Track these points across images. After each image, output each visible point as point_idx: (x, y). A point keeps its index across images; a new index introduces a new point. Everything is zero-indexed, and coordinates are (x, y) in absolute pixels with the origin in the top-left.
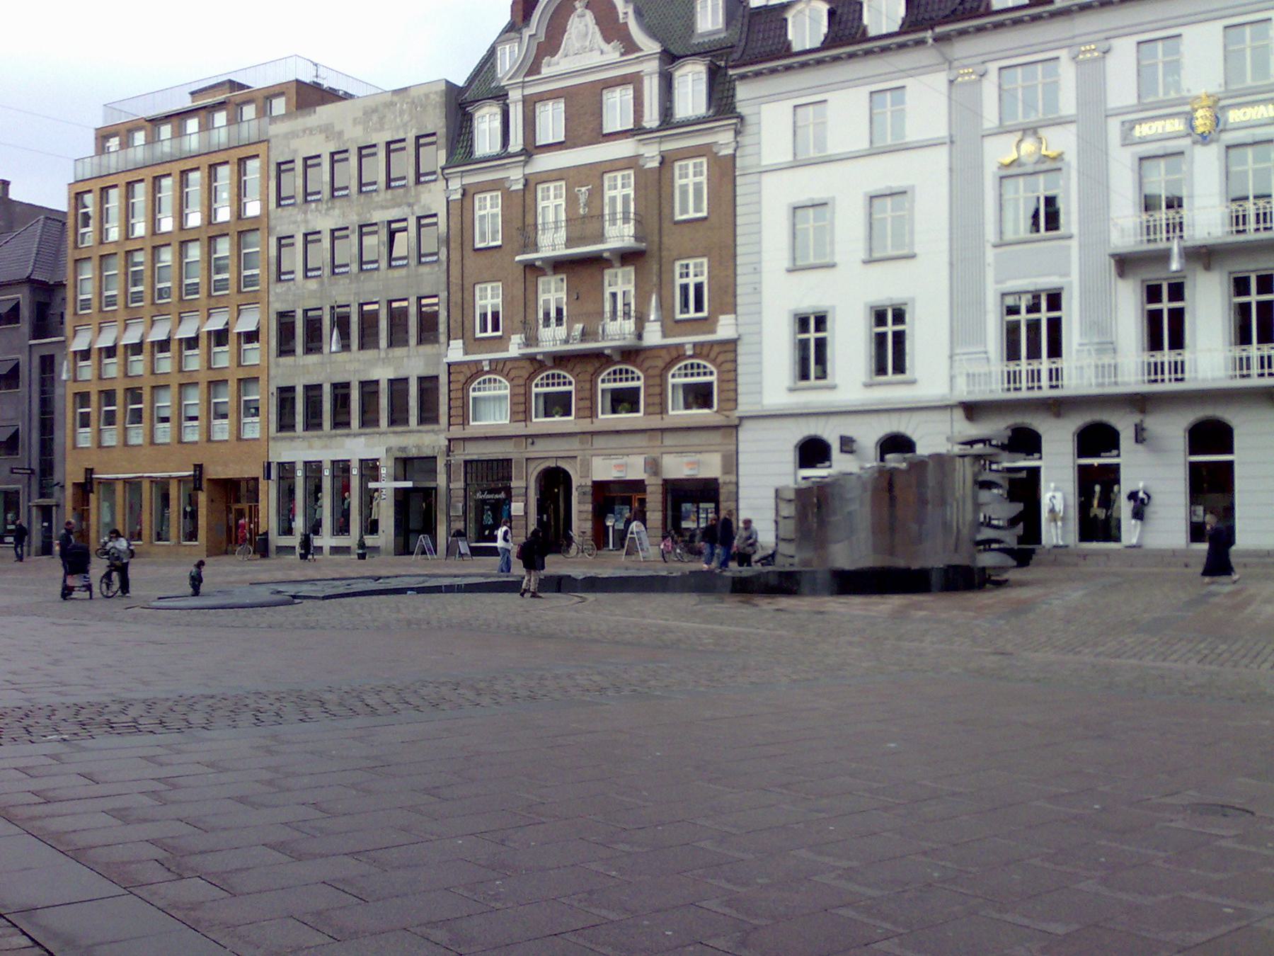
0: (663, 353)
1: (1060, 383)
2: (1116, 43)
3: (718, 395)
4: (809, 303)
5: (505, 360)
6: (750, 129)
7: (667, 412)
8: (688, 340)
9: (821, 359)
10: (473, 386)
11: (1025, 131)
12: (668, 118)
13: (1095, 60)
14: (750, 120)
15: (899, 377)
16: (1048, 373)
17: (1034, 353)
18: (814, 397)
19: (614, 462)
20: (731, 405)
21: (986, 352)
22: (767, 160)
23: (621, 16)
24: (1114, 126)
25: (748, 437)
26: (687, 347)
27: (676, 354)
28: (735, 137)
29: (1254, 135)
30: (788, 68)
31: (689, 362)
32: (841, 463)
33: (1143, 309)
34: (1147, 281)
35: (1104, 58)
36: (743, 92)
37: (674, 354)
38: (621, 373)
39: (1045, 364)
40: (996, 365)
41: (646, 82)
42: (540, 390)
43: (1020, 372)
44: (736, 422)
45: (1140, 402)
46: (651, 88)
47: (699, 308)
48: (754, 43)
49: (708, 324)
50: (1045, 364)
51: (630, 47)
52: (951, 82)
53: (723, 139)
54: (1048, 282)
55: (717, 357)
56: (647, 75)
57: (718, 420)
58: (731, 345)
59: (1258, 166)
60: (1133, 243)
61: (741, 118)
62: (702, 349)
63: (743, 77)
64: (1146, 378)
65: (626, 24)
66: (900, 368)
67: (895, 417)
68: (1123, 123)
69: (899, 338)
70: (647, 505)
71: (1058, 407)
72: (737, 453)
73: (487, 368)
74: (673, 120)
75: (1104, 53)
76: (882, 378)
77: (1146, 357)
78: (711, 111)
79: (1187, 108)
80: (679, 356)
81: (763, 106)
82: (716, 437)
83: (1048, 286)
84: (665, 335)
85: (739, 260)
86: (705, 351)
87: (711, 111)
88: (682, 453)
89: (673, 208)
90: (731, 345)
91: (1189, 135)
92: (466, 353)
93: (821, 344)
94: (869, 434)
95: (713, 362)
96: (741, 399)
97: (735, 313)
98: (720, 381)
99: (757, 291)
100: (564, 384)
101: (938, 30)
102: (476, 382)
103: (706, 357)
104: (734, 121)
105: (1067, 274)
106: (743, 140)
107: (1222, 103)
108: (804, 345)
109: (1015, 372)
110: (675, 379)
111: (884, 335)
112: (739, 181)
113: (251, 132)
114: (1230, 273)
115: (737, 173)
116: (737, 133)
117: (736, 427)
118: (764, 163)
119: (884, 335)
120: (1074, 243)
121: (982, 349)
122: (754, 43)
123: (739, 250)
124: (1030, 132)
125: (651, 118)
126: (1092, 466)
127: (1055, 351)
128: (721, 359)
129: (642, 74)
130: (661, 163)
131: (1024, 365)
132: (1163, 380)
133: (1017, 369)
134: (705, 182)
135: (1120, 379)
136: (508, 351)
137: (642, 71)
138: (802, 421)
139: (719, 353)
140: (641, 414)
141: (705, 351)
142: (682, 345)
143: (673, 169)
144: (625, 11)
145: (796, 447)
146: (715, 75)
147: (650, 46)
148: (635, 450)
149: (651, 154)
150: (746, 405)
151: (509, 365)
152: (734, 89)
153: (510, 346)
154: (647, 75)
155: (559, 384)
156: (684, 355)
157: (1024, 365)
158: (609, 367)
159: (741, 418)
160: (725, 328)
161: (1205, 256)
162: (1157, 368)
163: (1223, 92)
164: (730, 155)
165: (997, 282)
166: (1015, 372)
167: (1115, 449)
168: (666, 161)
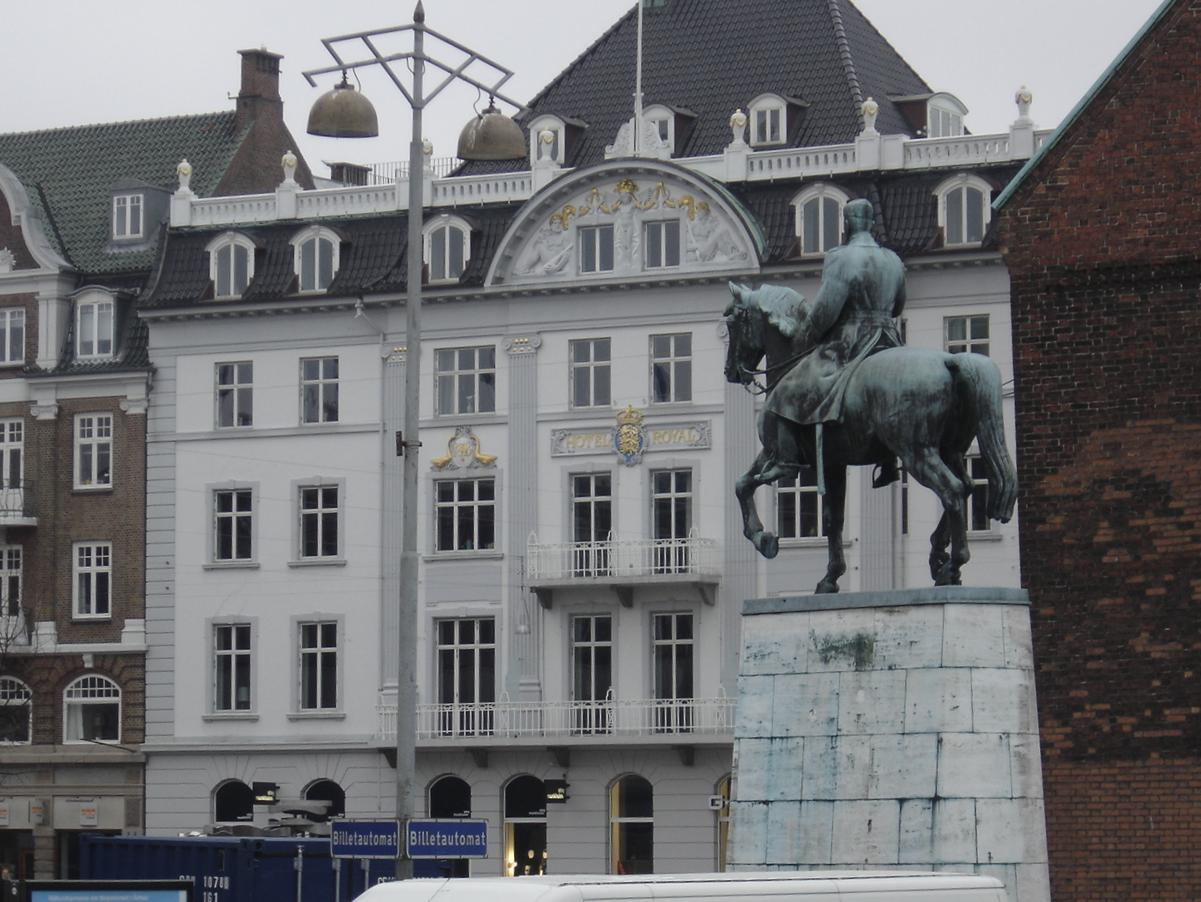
0: (58, 664)
1: (607, 728)
2: (548, 338)
3: (123, 724)
4: (231, 612)
5: (116, 656)
6: (163, 386)
7: (61, 743)
8: (87, 648)
9: (244, 680)
10: (68, 688)
11: (458, 428)
12: (68, 357)
13: (527, 356)
14: (163, 374)
15: (328, 711)
16: (212, 725)
17: (467, 696)
18: (236, 733)
19: (85, 805)
20: (137, 736)
21: (539, 685)
22: (183, 427)
23: (13, 219)
24: (545, 433)
25: (157, 777)
26: (85, 658)
27: (71, 666)
28: (147, 395)
29: (674, 460)
30: (208, 317)
31: (88, 676)
32: (260, 818)
33: (570, 648)
34: (656, 612)
35: (536, 353)
36: (157, 339)
37: (70, 665)
38: (93, 685)
39: (477, 707)
40: (427, 708)
41: (42, 309)
42: (75, 700)
43: (473, 713)
44: (143, 759)
45: (563, 755)
46: (49, 318)
47: (102, 608)
48: (344, 282)
49: (108, 630)
50: (477, 707)
51: (24, 260)
52: (384, 360)
53: (132, 394)
54: (477, 608)
55: (121, 673)
56: (43, 299)
57: (119, 755)
58: (138, 659)
59: (673, 501)
60: (560, 575)
61: (154, 371)
62: (103, 661)
63: (156, 320)
64: (654, 727)
65: (19, 228)
66: (330, 700)
67: (322, 760)
68: (554, 432)
69: (330, 661)
70: (36, 863)
71: (482, 757)
72: (144, 799)
73: (88, 665)
74: (74, 363)
75: (537, 349)
76: (311, 712)
77: (654, 704)
78: (120, 355)
79: (614, 423)
80: (76, 669)
81: (179, 358)
82: (118, 779)
83: (462, 615)
84: (60, 641)
85: (150, 550)
86: (108, 664)
87: (120, 355)
88: (78, 796)
89: (71, 474)
90: (137, 660)
91: (614, 453)
92: (60, 641)
93: (244, 663)
94: (293, 782)
95: (116, 678)
96: (149, 729)
97: (144, 618)
98: (126, 704)
99: (169, 591)
100: (108, 694)
101: (368, 299)
102: (73, 684)
103: (108, 673)
104: (145, 375)
105: (497, 602)
106: (155, 398)
107: (646, 422)
108: (225, 662)
109: (468, 713)
110: (73, 698)
111: (313, 656)
112: (151, 449)
113: (45, 306)
114: (651, 613)
115: (149, 439)
116: (150, 389)
117: (144, 765)
118: (179, 431)
119: (313, 656)
120: (504, 565)
121: (536, 681)
122: (344, 282)
123: (150, 537)
124: (464, 431)
125: (48, 357)
126: (248, 840)
127: (488, 695)
128: (126, 676)
129: (37, 297)
130: (58, 415)
131: (456, 708)
132: (670, 731)
133: (588, 707)
134: (22, 448)
135: (545, 729)
136: (119, 641)
137: (38, 293)
138: (220, 762)
139: (123, 668)
140: (29, 742)
141: (108, 664)
142: (79, 656)
143: (72, 423)
144: (18, 214)
145: (213, 792)
146: (125, 308)
147: (50, 261)
148: (21, 791)
149: (46, 405)
150: (152, 742)
151: (121, 663)
152: (147, 338)
153: (123, 635)
154: (43, 299)
155: (100, 694)
156: (83, 667)
157: (456, 708)
158: (78, 676)
159: (148, 755)
160: (132, 637)
161: (627, 594)
162: (664, 716)
163: (647, 409)
164: (140, 414)
165: (429, 604)
166: (468, 713)
167: (466, 809)
168: (65, 411)
